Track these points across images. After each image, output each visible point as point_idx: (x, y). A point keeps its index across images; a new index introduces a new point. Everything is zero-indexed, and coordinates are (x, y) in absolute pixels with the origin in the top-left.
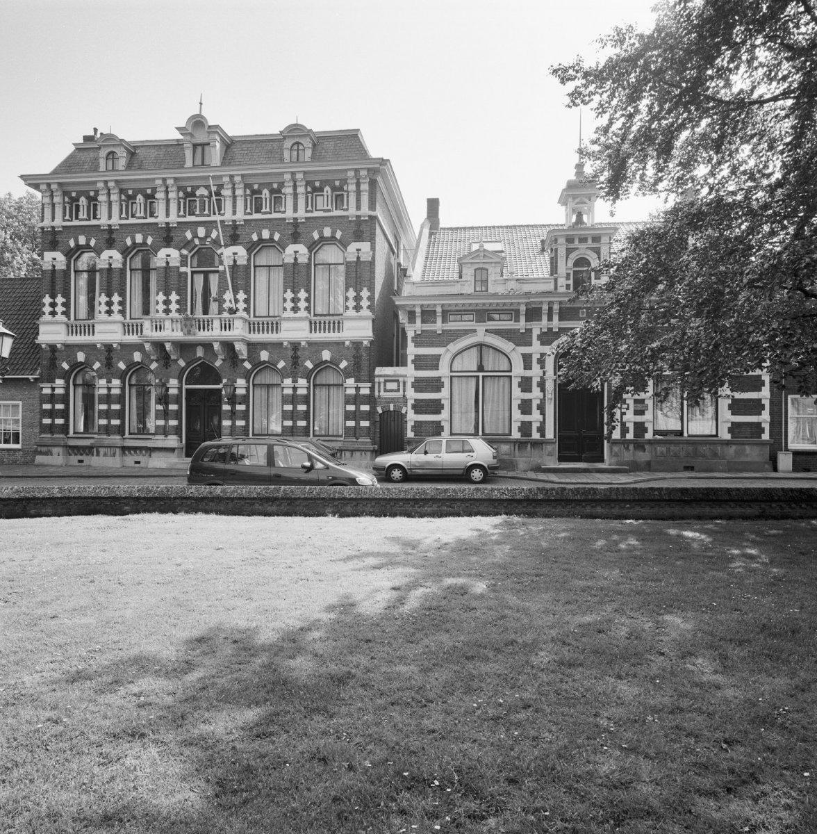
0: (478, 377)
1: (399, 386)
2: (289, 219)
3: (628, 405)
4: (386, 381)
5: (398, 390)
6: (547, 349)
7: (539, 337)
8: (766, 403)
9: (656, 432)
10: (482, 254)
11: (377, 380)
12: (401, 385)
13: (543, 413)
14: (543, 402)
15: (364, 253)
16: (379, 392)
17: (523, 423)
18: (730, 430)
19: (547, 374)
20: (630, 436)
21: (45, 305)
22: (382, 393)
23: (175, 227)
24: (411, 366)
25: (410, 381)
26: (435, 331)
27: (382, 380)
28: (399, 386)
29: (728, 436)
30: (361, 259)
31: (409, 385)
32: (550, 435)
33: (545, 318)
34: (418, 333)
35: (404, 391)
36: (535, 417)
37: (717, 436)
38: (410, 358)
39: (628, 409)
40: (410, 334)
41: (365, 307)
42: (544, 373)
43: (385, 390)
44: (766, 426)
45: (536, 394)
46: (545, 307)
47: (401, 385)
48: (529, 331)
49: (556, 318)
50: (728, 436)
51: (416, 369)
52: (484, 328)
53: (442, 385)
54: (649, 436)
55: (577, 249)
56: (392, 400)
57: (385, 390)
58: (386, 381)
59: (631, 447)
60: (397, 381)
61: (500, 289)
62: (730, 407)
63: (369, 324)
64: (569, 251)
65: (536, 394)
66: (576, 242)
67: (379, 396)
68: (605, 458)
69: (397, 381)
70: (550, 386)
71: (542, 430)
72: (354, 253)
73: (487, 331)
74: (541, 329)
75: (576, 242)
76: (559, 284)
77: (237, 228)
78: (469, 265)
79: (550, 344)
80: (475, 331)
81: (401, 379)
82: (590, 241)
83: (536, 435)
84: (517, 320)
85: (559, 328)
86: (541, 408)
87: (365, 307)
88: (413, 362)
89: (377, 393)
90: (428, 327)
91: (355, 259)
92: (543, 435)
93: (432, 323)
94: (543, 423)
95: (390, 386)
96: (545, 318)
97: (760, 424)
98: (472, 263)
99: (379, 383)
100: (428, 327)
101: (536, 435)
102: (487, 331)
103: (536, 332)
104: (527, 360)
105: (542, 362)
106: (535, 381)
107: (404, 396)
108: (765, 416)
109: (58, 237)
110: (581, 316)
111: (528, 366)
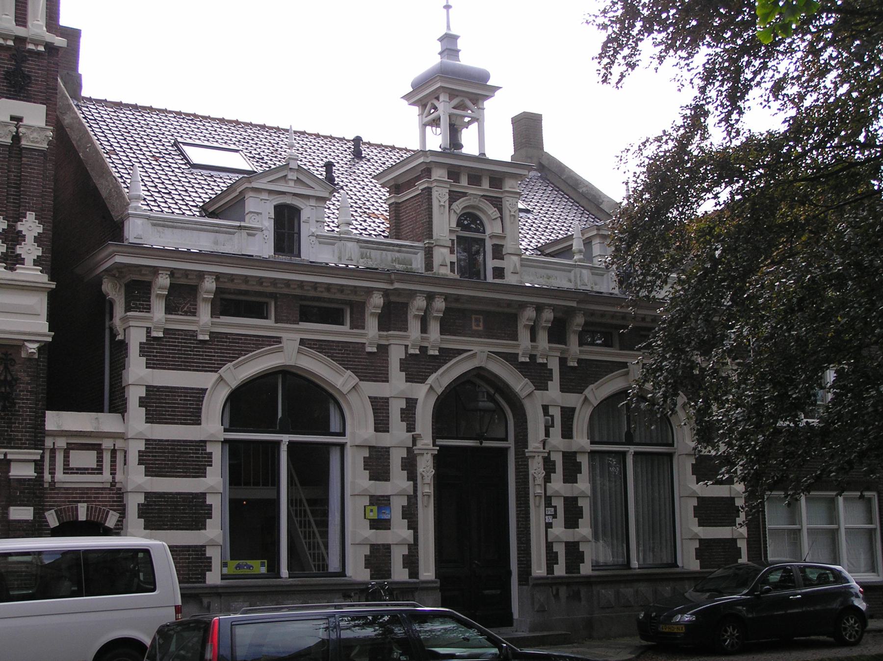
0: (624, 454)
1: (100, 460)
2: (36, 43)
3: (555, 507)
4: (70, 447)
5: (99, 470)
6: (420, 391)
7: (405, 365)
8: (217, 504)
9: (596, 566)
10: (292, 176)
11: (49, 442)
12: (107, 457)
13: (413, 526)
14: (412, 499)
15: (28, 127)
16: (52, 473)
17: (374, 547)
18: (699, 554)
19: (419, 445)
20: (560, 570)
21: (38, 240)
22: (60, 476)
23: (39, 53)
24: (136, 413)
25: (135, 448)
26: (193, 334)
27: (61, 443)
28: (100, 460)
29: (694, 565)
30: (24, 143)
31: (133, 457)
32: (428, 572)
33: (414, 327)
34: (154, 334)
35: (113, 473)
36: (399, 532)
37: (343, 574)
38: (134, 395)
39: (555, 516)
40: (136, 338)
41: (29, 259)
42: (414, 440)
43: (67, 470)
44: (742, 545)
45: (398, 482)
46: (420, 302)
47: (107, 457)
48: (383, 350)
49: (434, 328)
50: (694, 565)
51: (149, 420)
52: (298, 337)
53: (208, 459)
54: (586, 569)
55: (465, 194)
56: (85, 494)
57: (67, 470)
58: (70, 447)
59: (563, 591)
60: (98, 448)
61: (326, 256)
62: (697, 511)
63: (40, 303)
64: (454, 197)
65: (398, 482)
66: (464, 181)
67: (53, 482)
68: (516, 616)
69: (98, 448)
70: (426, 467)
71: (411, 562)
72: (6, 124)
73: (302, 342)
74: (149, 330)
75: (464, 181)
76: (437, 260)
77: (24, 60)
78: (265, 196)
79: (423, 381)
80: (278, 340)
81: (107, 444)
82: (486, 185)
83: (399, 574)
84: (358, 323)
85: (441, 350)
86: (410, 515)
87: (29, 259)
88: (142, 402)
89: (47, 477)
90: (180, 323)
91: (9, 140)
92: (414, 573)
93: (186, 313)
94: (413, 547)
95: (84, 459)
96: (414, 327)
97: (734, 541)
98: (271, 192)
99: (53, 451)
100: (180, 323)
101: (399, 574)
102: (302, 342)
103: (396, 355)
104: (380, 407)
105: (409, 413)
106: (396, 458)
107: (113, 483)
108: (740, 531)
109: (30, 67)
110: (474, 328)
111: (382, 425)
